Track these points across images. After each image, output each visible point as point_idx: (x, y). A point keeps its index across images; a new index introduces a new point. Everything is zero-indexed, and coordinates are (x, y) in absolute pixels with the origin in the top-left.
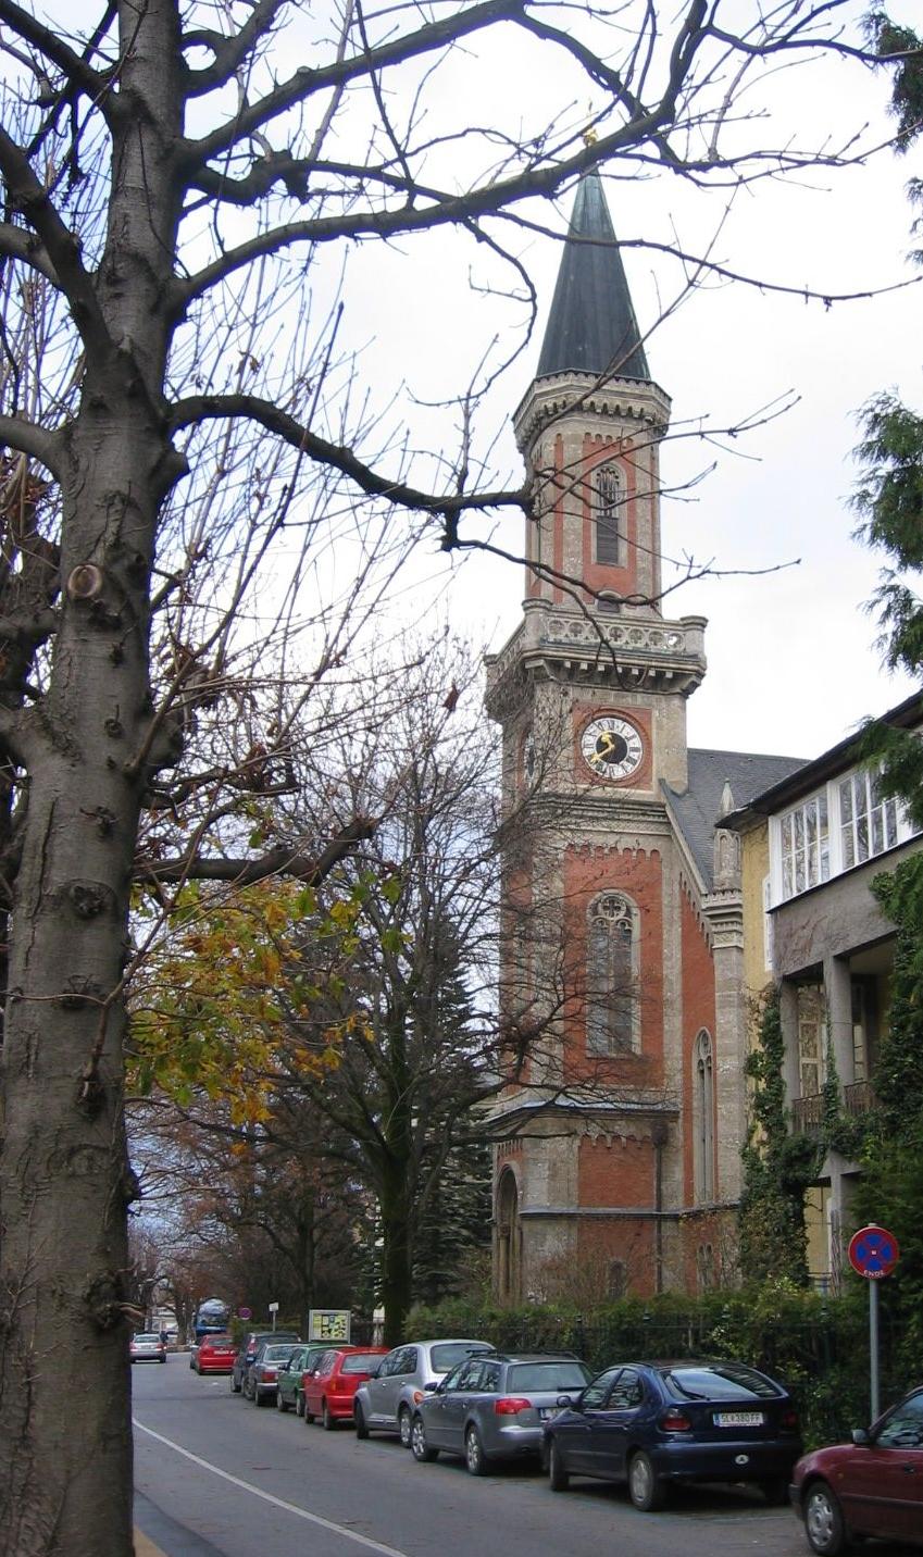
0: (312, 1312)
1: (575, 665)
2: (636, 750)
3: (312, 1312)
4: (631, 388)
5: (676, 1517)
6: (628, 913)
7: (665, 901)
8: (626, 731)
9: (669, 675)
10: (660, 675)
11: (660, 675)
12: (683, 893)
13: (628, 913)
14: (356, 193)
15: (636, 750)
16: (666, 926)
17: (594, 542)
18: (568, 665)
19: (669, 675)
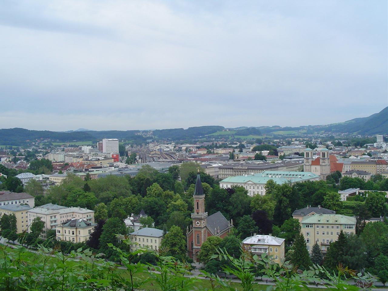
8: (199, 222)
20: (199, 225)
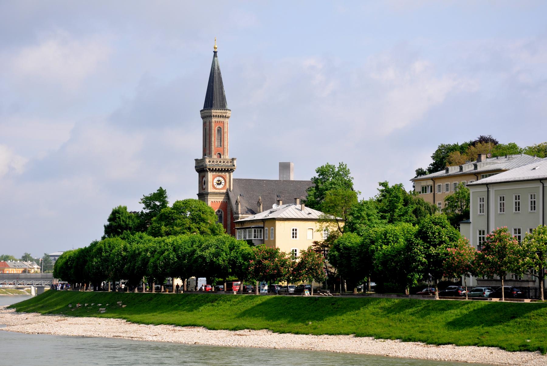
0: (205, 279)
1: (213, 169)
2: (223, 183)
3: (205, 279)
4: (223, 111)
5: (305, 222)
6: (222, 213)
7: (228, 210)
8: (221, 179)
9: (229, 169)
10: (228, 169)
11: (228, 169)
12: (231, 210)
13: (222, 213)
14: (204, 220)
15: (223, 183)
16: (228, 215)
17: (216, 143)
18: (211, 169)
19: (229, 169)
20: (221, 186)
